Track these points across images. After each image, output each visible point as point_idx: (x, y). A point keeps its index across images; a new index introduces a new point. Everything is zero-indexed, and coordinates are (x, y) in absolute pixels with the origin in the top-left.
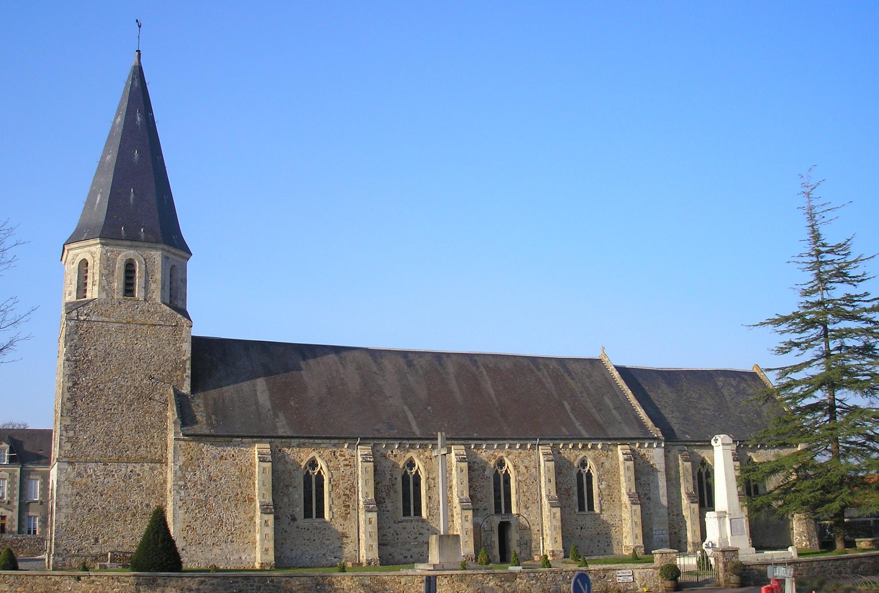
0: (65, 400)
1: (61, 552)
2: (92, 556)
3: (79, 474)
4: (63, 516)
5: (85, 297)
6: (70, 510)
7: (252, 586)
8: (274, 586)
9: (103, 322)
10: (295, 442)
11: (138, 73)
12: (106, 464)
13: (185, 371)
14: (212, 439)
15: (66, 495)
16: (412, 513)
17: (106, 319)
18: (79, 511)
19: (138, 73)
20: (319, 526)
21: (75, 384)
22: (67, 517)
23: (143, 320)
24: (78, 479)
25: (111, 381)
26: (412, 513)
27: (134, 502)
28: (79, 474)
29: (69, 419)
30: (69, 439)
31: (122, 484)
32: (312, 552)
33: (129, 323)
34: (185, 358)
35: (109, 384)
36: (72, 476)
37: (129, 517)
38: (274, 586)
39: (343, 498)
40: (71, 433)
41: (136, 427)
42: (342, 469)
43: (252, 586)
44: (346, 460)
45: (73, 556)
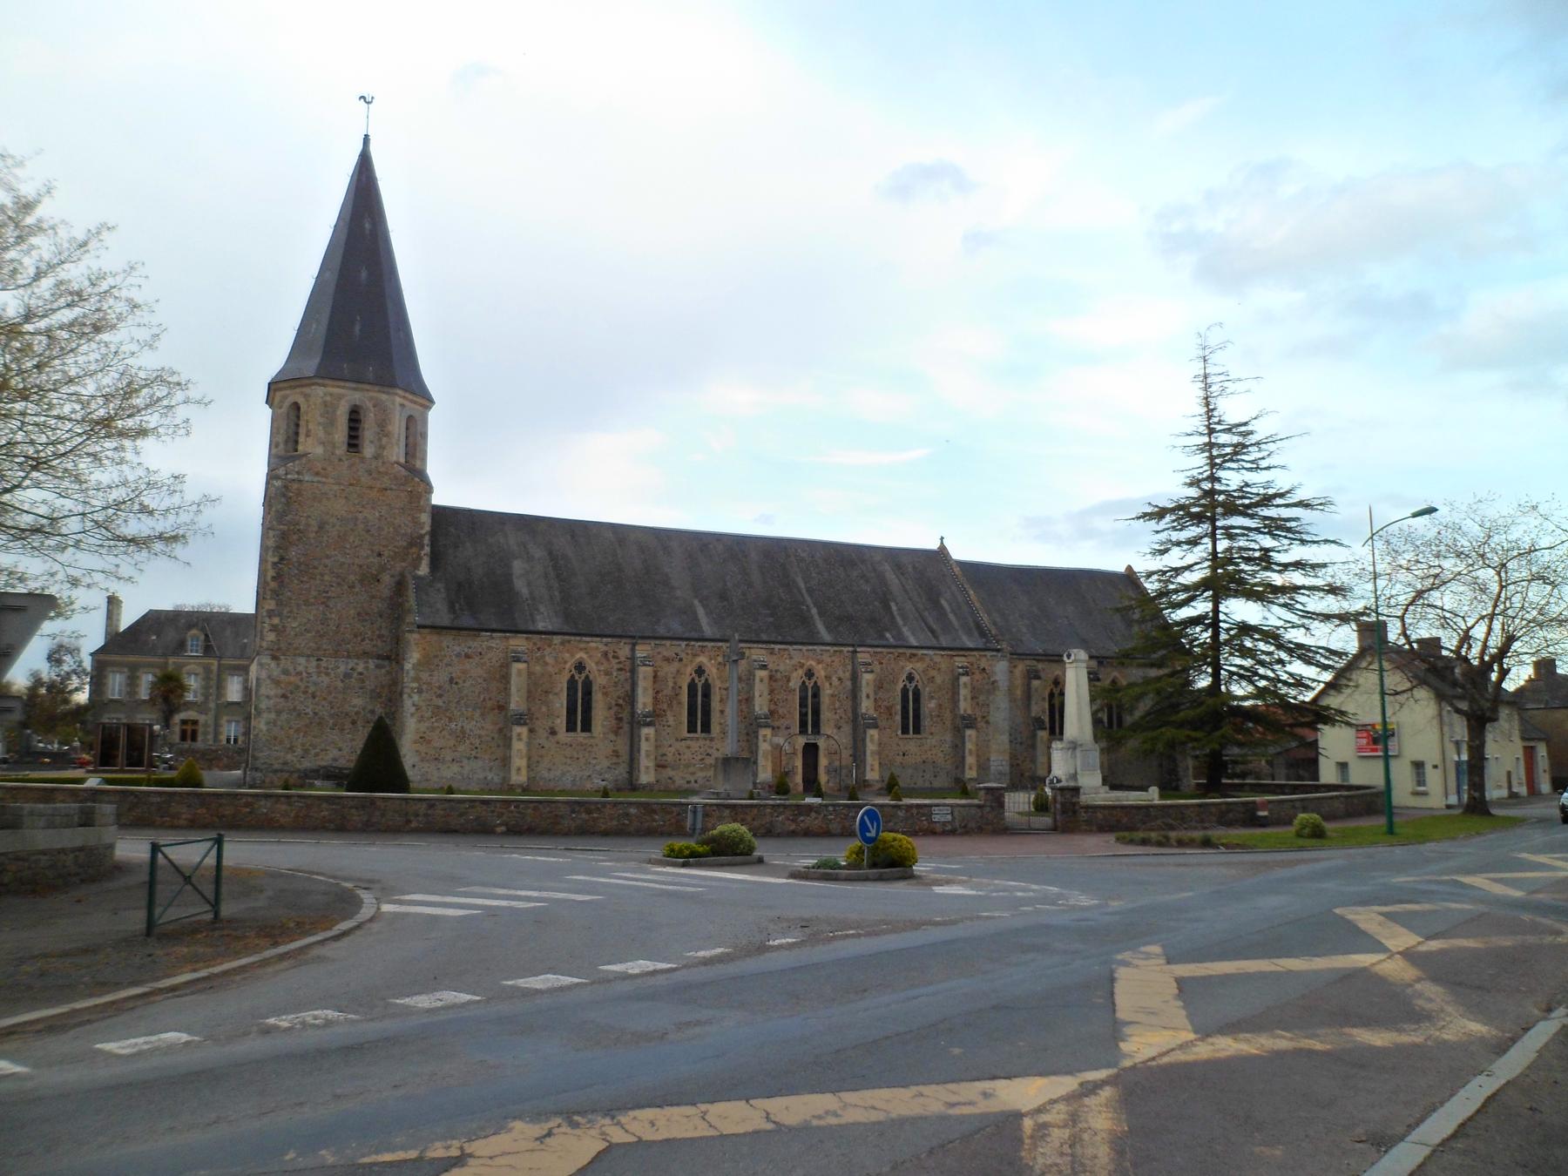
2: (298, 771)
6: (273, 716)
10: (557, 639)
13: (422, 547)
18: (284, 716)
21: (282, 559)
24: (283, 677)
25: (328, 557)
28: (286, 672)
30: (274, 628)
31: (340, 685)
35: (327, 561)
37: (348, 726)
40: (276, 621)
45: (276, 771)
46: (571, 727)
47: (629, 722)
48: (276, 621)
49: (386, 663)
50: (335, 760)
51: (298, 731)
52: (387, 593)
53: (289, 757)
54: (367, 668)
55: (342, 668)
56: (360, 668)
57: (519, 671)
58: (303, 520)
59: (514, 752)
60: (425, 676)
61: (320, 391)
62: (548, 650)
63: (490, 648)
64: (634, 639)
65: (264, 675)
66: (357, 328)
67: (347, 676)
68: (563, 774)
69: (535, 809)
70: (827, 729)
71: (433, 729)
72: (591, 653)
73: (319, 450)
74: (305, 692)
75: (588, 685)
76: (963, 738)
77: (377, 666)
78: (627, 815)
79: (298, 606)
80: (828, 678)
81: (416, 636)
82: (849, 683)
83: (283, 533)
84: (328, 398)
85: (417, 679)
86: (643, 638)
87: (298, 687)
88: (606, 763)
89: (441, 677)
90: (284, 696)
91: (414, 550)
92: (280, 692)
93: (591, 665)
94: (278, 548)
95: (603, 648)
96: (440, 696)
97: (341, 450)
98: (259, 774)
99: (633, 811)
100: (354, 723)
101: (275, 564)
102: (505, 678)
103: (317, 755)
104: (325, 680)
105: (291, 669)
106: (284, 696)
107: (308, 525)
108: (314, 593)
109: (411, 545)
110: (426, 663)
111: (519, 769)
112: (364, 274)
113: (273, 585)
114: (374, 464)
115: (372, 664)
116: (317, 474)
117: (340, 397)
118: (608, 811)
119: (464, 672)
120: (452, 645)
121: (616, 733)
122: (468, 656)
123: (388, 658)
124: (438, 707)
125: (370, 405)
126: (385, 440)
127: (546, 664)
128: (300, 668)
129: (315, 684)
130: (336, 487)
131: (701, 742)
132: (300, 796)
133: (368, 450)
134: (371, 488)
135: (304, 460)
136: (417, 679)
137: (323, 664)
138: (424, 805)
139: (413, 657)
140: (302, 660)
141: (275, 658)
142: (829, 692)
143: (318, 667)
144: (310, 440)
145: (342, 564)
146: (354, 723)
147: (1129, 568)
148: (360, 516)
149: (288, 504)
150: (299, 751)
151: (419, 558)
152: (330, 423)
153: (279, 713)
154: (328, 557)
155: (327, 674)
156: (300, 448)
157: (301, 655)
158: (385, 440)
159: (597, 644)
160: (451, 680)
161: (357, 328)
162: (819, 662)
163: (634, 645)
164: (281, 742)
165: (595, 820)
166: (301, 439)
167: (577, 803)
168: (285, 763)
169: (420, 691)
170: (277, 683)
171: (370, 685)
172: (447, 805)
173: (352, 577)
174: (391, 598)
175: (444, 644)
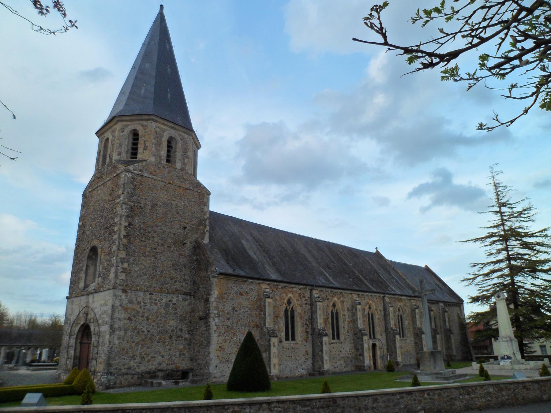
0: (122, 236)
1: (113, 371)
2: (138, 373)
3: (131, 302)
4: (116, 338)
5: (136, 158)
6: (122, 333)
7: (415, 400)
8: (430, 399)
9: (152, 178)
10: (281, 285)
11: (161, 20)
12: (151, 294)
13: (205, 227)
14: (235, 278)
15: (120, 319)
16: (290, 339)
17: (155, 177)
18: (129, 333)
19: (161, 20)
20: (294, 346)
21: (130, 224)
22: (119, 339)
23: (179, 184)
24: (129, 305)
25: (156, 226)
26: (290, 339)
27: (171, 326)
28: (131, 302)
29: (124, 253)
30: (124, 271)
31: (163, 311)
32: (290, 366)
33: (170, 183)
34: (206, 217)
35: (155, 229)
36: (124, 303)
37: (167, 340)
38: (430, 399)
39: (306, 326)
40: (126, 265)
41: (173, 265)
42: (304, 306)
43: (415, 400)
44: (306, 300)
45: (124, 374)
46: (287, 339)
47: (315, 336)
48: (126, 265)
49: (188, 297)
50: (160, 364)
51: (138, 344)
52: (187, 253)
53: (132, 363)
54: (178, 301)
55: (164, 301)
56: (174, 301)
57: (269, 303)
58: (143, 201)
59: (272, 355)
60: (221, 306)
61: (154, 124)
62: (277, 292)
63: (251, 289)
64: (312, 286)
65: (117, 303)
66: (169, 96)
67: (167, 305)
68: (286, 367)
69: (439, 395)
70: (378, 336)
71: (225, 341)
72: (294, 294)
73: (153, 159)
74: (143, 316)
75: (293, 311)
76: (421, 339)
77: (185, 300)
78: (489, 393)
79: (139, 256)
80: (376, 309)
81: (216, 280)
82: (383, 312)
83: (131, 207)
84: (158, 129)
85: (217, 308)
86: (316, 286)
87: (138, 312)
88: (303, 359)
89: (228, 307)
90: (130, 319)
91: (201, 227)
92: (127, 316)
93: (295, 302)
94: (128, 216)
95: (299, 292)
96: (228, 319)
97: (164, 162)
98: (113, 377)
99: (491, 390)
100: (171, 337)
101: (126, 227)
102: (262, 309)
103: (149, 361)
104: (154, 307)
105: (134, 299)
106: (130, 319)
107: (146, 204)
108: (149, 249)
109: (200, 224)
110: (221, 298)
111: (275, 365)
112: (169, 70)
113: (125, 241)
114: (181, 172)
115: (181, 298)
116: (151, 173)
117: (164, 131)
118: (479, 392)
119: (239, 304)
120: (234, 287)
121: (306, 341)
122: (241, 294)
123: (189, 294)
124: (228, 326)
125: (178, 138)
126: (186, 160)
127: (276, 300)
128: (140, 299)
129: (149, 310)
130: (161, 183)
131: (338, 344)
132: (279, 402)
133: (179, 165)
134: (180, 187)
135: (144, 164)
136: (217, 308)
137: (154, 297)
138: (371, 399)
139: (215, 293)
140: (141, 294)
141: (125, 291)
142: (377, 317)
143: (150, 299)
144: (147, 152)
145: (164, 232)
146: (171, 337)
147: (426, 266)
148: (174, 203)
149: (134, 189)
150: (138, 359)
151: (204, 233)
152: (158, 145)
153: (126, 331)
154: (156, 226)
155: (156, 304)
156: (139, 156)
157: (140, 290)
158: (186, 160)
159: (296, 288)
160: (234, 308)
161: (169, 96)
162: (373, 302)
163: (311, 290)
164: (127, 352)
165: (472, 398)
166: (140, 151)
167: (462, 387)
168: (129, 368)
169: (219, 316)
170: (126, 309)
171: (179, 311)
172: (385, 398)
173: (169, 241)
174: (190, 256)
175: (230, 286)
